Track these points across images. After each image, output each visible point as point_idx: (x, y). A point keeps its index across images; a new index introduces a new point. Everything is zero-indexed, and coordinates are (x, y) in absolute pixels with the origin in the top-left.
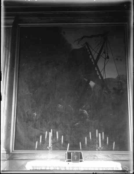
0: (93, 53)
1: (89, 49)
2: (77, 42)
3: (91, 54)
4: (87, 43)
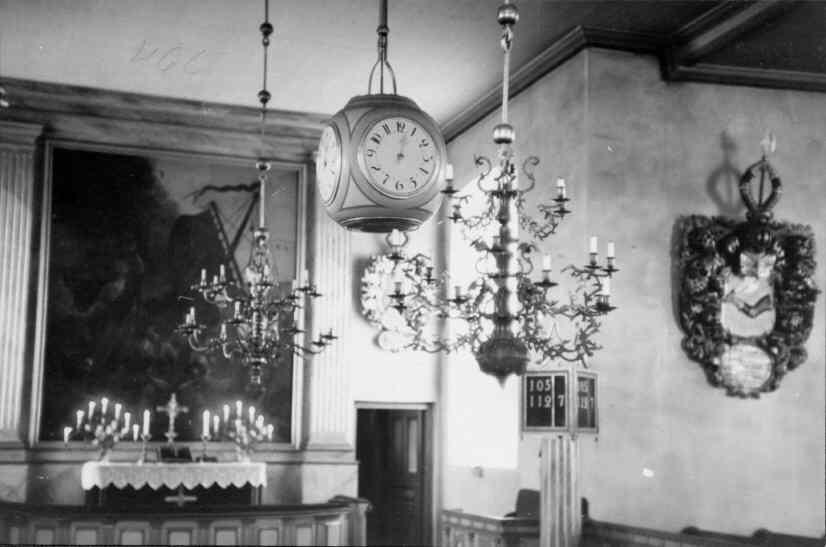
0: (227, 227)
1: (218, 217)
2: (192, 198)
3: (222, 229)
4: (213, 204)
